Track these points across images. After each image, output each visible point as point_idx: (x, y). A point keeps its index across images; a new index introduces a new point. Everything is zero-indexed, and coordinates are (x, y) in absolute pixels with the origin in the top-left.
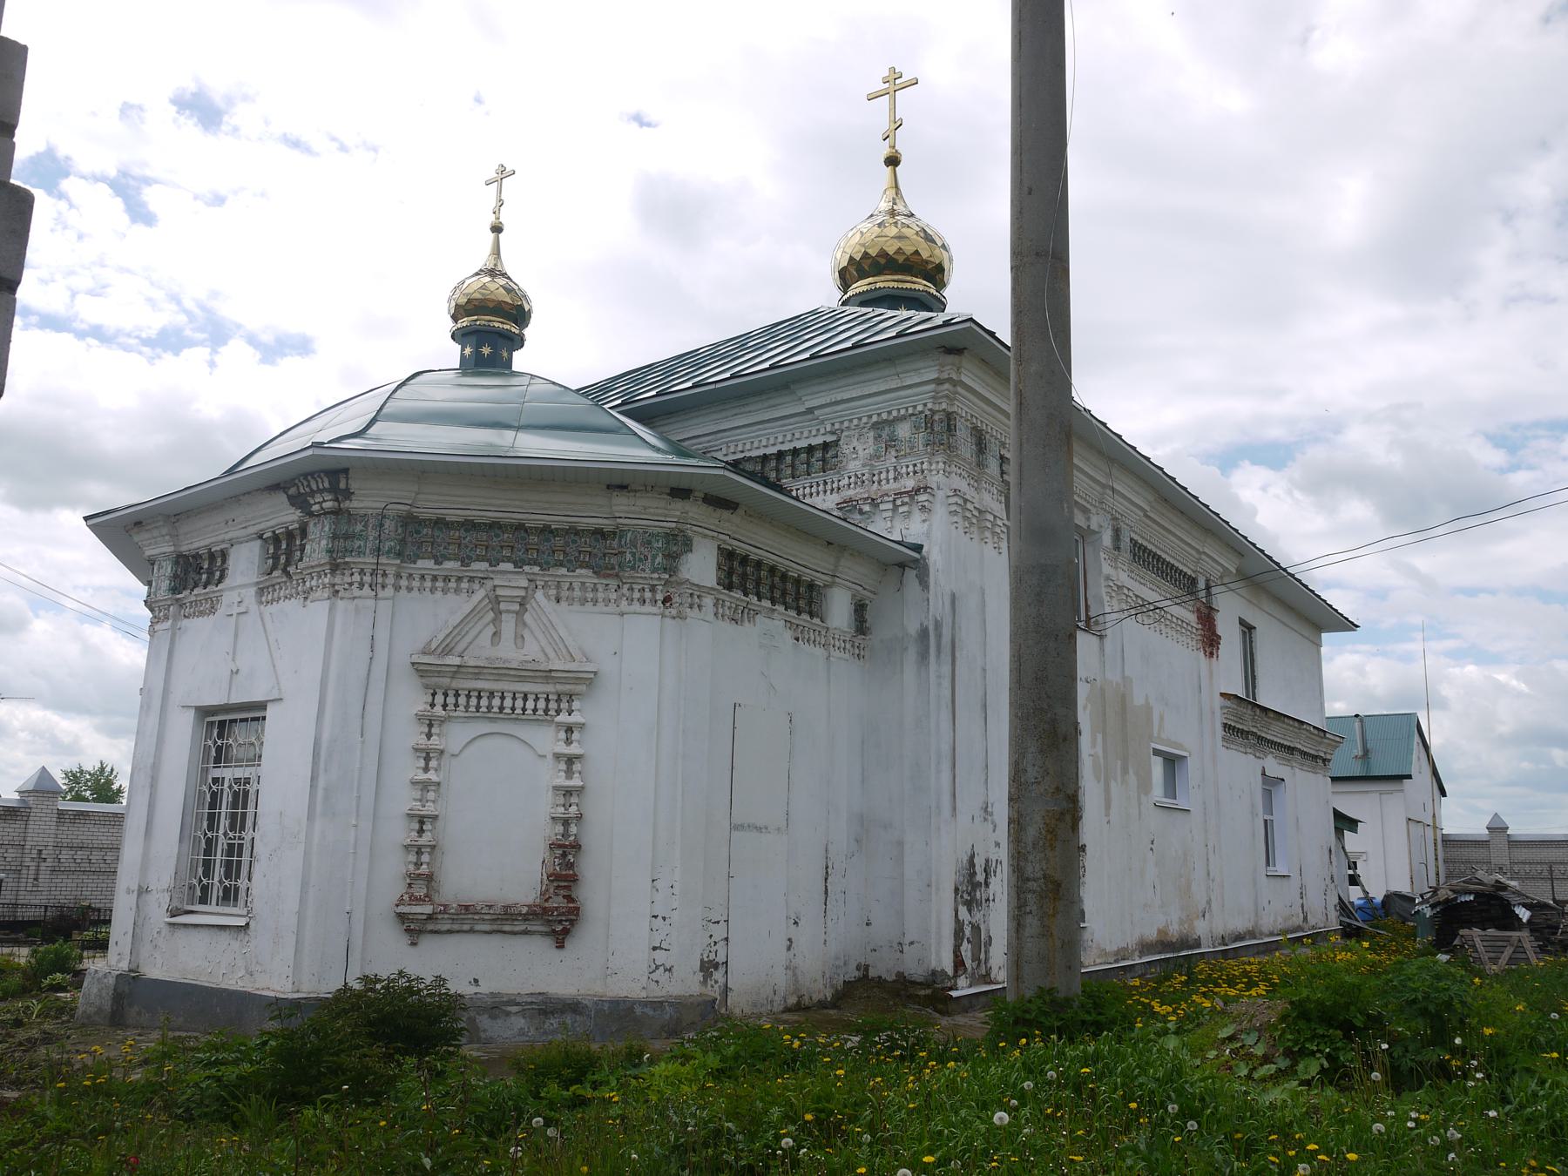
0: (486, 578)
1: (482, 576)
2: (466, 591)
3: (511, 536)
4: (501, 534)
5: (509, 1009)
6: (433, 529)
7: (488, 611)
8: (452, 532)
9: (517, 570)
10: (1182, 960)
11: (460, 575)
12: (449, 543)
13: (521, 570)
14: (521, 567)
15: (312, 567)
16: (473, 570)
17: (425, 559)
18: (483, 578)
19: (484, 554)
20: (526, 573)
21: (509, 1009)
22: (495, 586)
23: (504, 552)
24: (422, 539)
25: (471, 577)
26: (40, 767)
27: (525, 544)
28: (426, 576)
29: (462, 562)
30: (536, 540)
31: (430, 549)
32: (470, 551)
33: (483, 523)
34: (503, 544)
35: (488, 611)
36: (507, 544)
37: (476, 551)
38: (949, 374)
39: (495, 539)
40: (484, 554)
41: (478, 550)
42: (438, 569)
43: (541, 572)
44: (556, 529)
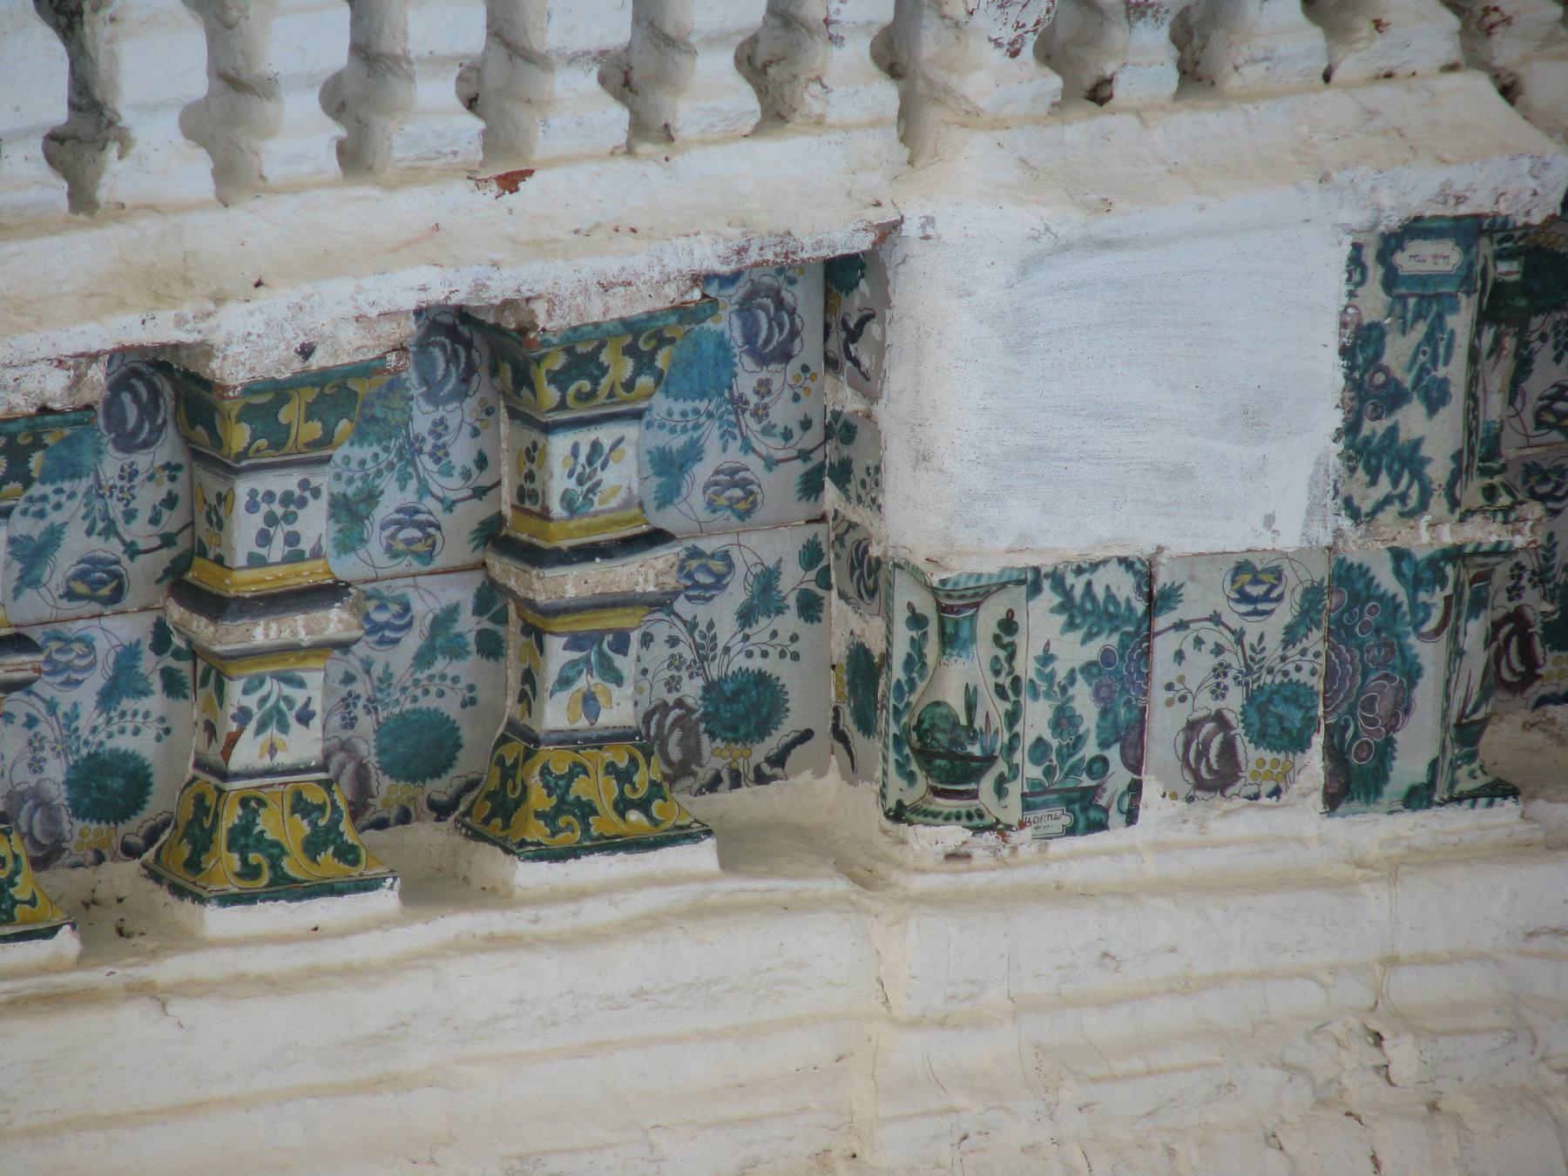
8: (619, 711)
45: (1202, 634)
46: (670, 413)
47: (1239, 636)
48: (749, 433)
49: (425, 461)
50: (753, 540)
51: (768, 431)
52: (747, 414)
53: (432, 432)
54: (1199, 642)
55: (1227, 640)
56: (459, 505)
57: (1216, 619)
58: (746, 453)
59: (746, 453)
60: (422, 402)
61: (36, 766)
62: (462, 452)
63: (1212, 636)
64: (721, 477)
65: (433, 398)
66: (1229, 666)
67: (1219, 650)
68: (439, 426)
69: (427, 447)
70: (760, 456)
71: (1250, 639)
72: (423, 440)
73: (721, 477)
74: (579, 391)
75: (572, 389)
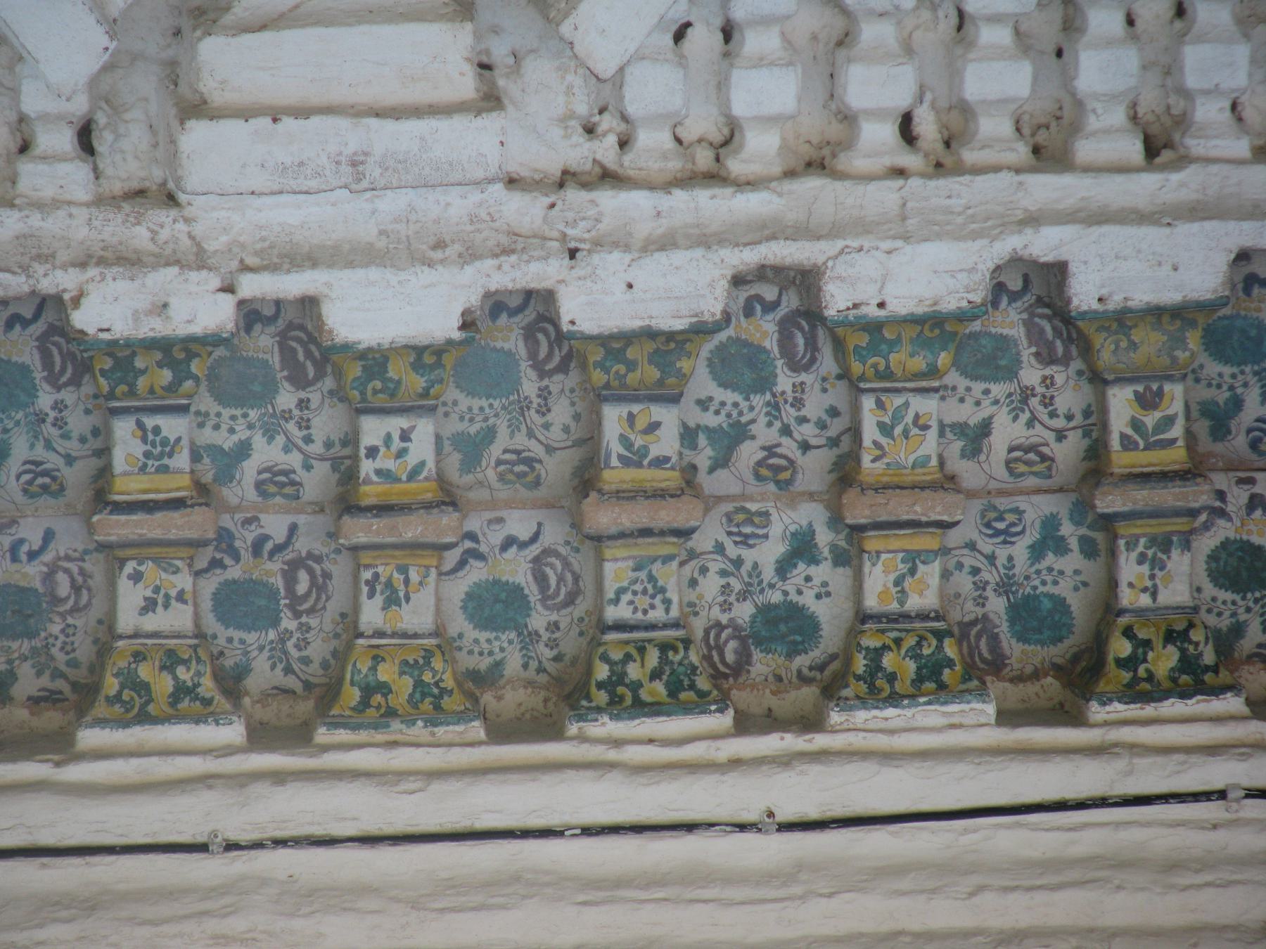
0: (566, 179)
1: (609, 201)
2: (755, 42)
3: (372, 614)
4: (459, 624)
5: (317, 354)
6: (1109, 609)
7: (384, 509)
8: (923, 598)
9: (291, 285)
10: (185, 648)
11: (812, 184)
12: (948, 482)
13: (253, 286)
14: (251, 314)
15: (652, 627)
16: (705, 240)
17: (1157, 313)
18: (608, 177)
19: (613, 417)
20: (199, 260)
21: (317, 354)
22: (491, 100)
23: (422, 449)
24: (1198, 495)
25: (715, 177)
26: (1063, 258)
27: (224, 539)
28: (1133, 149)
29: (812, 315)
30: (130, 597)
31: (1121, 403)
32: (739, 433)
33: (643, 708)
34: (444, 525)
35: (384, 509)
36: (412, 528)
37: (689, 435)
38: (1133, 346)
39: (516, 570)
40: (613, 417)
41: (667, 443)
42: (1033, 220)
43: (62, 281)
44: (205, 713)
45: (962, 560)
46: (470, 409)
47: (991, 558)
48: (533, 427)
49: (49, 430)
50: (735, 489)
51: (66, 436)
52: (532, 412)
53: (53, 408)
54: (960, 566)
55: (980, 563)
56: (558, 452)
57: (972, 546)
58: (529, 439)
59: (529, 439)
60: (286, 384)
61: (981, 601)
62: (78, 423)
63: (968, 562)
64: (508, 456)
65: (53, 381)
66: (987, 583)
67: (975, 571)
68: (58, 406)
69: (50, 420)
70: (541, 443)
71: (1001, 560)
72: (47, 415)
73: (508, 456)
74: (374, 389)
75: (370, 386)
